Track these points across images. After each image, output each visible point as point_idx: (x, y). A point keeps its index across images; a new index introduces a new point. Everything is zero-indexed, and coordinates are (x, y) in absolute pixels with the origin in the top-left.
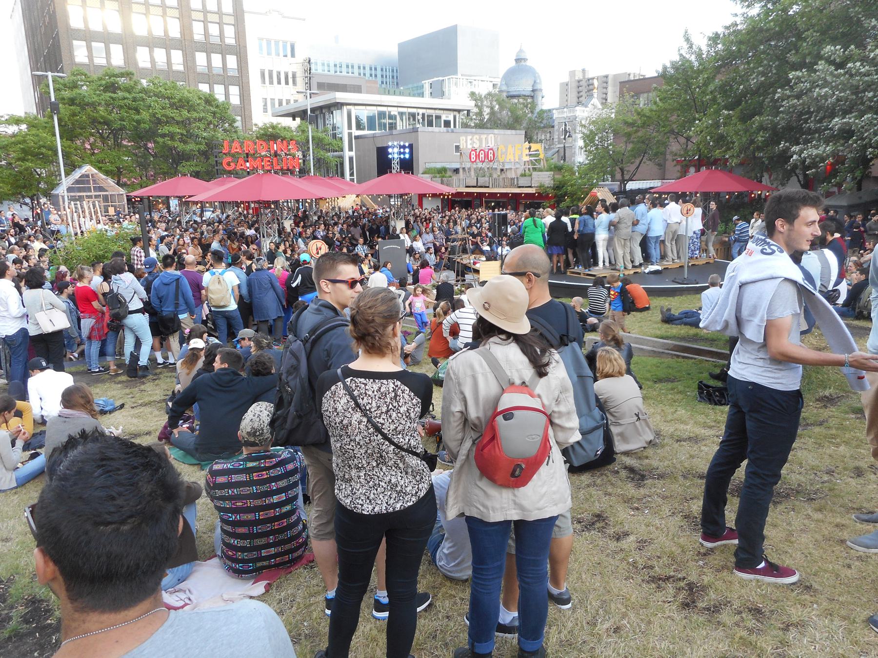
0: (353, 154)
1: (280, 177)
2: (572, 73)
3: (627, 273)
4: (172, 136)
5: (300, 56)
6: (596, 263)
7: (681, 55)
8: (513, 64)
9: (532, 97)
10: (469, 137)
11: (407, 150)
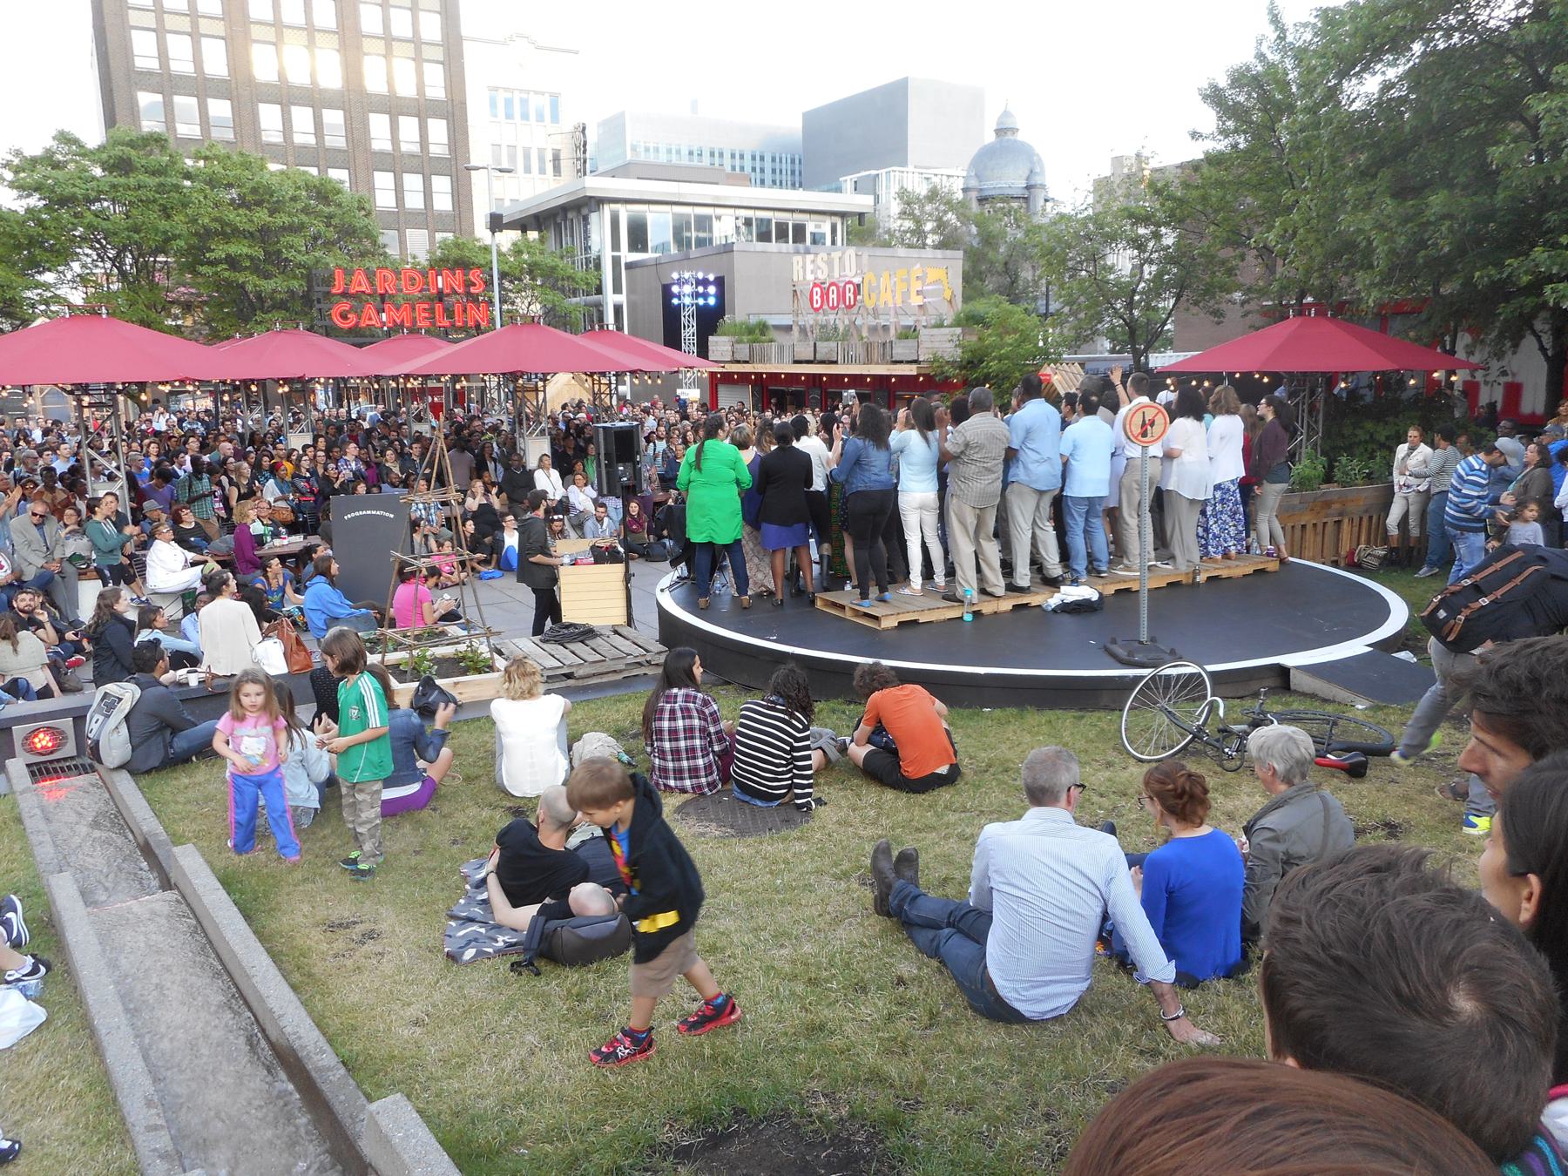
0: (622, 298)
1: (136, 327)
2: (1117, 161)
3: (988, 607)
4: (233, 262)
5: (568, 123)
6: (895, 571)
7: (1261, 57)
8: (990, 137)
9: (1026, 199)
10: (810, 257)
11: (712, 290)
